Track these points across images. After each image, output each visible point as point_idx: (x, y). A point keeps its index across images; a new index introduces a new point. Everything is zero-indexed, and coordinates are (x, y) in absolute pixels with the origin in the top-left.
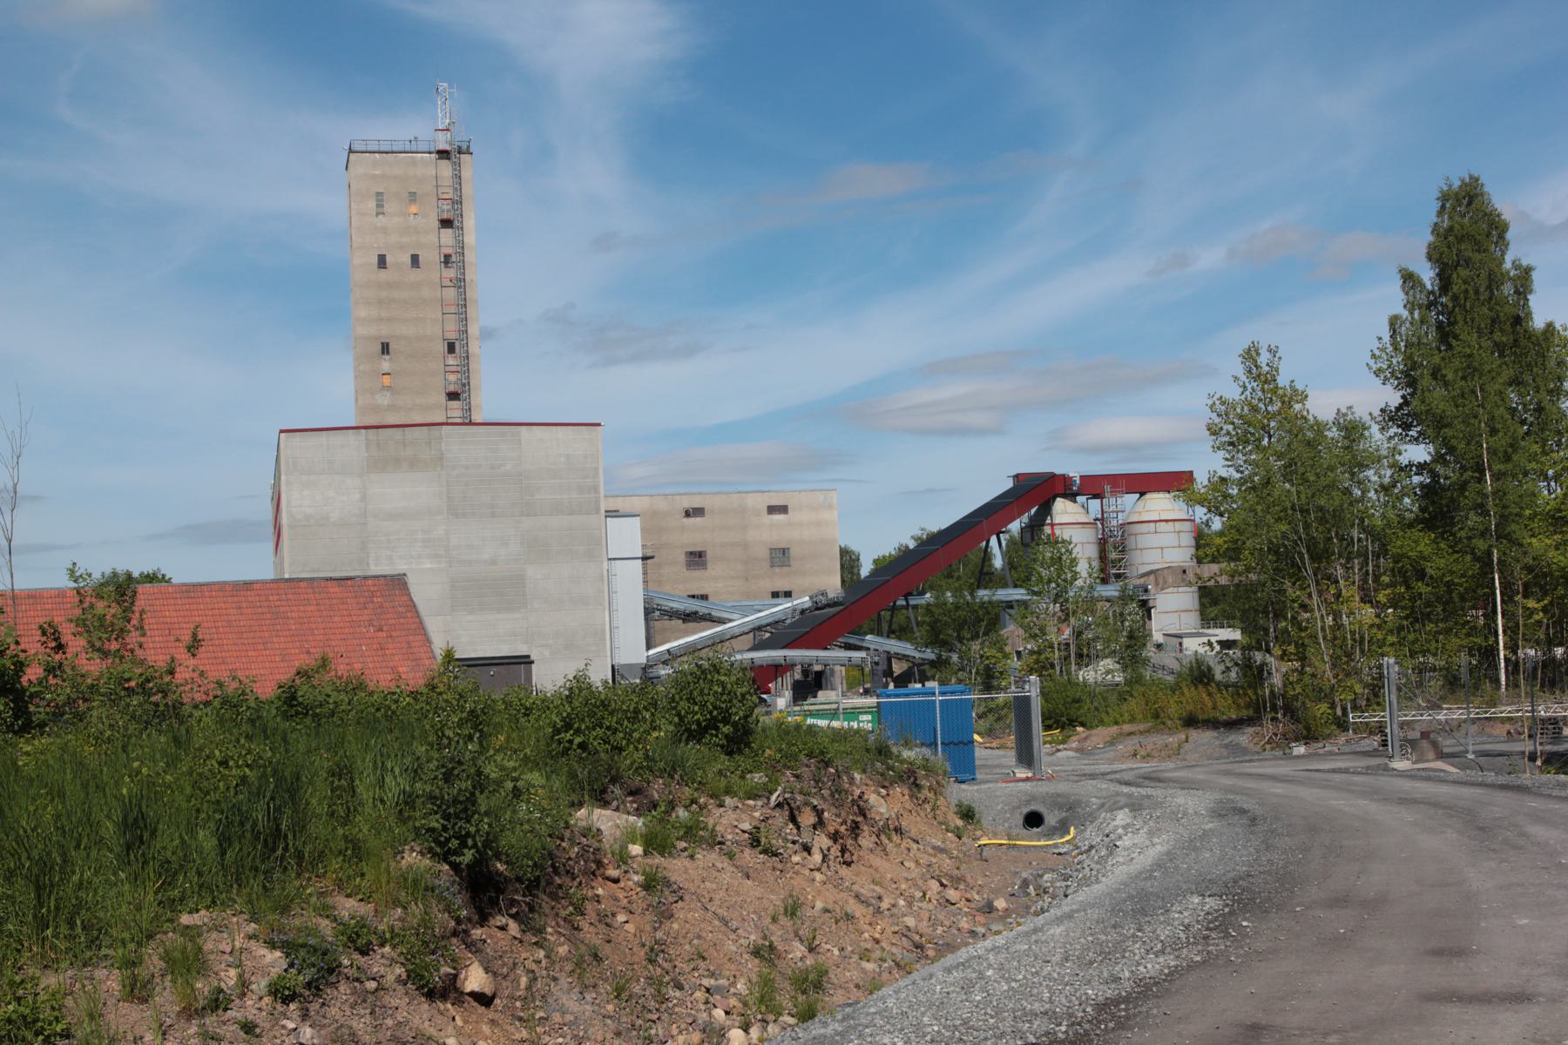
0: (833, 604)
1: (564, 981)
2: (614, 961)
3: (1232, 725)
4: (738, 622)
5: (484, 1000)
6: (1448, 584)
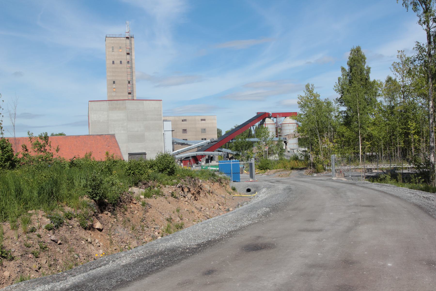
0: (216, 141)
1: (120, 226)
2: (133, 221)
3: (301, 169)
4: (194, 145)
5: (100, 230)
6: (350, 138)
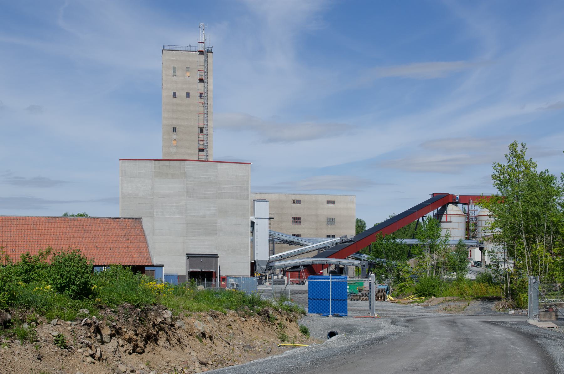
0: (350, 241)
4: (310, 246)
